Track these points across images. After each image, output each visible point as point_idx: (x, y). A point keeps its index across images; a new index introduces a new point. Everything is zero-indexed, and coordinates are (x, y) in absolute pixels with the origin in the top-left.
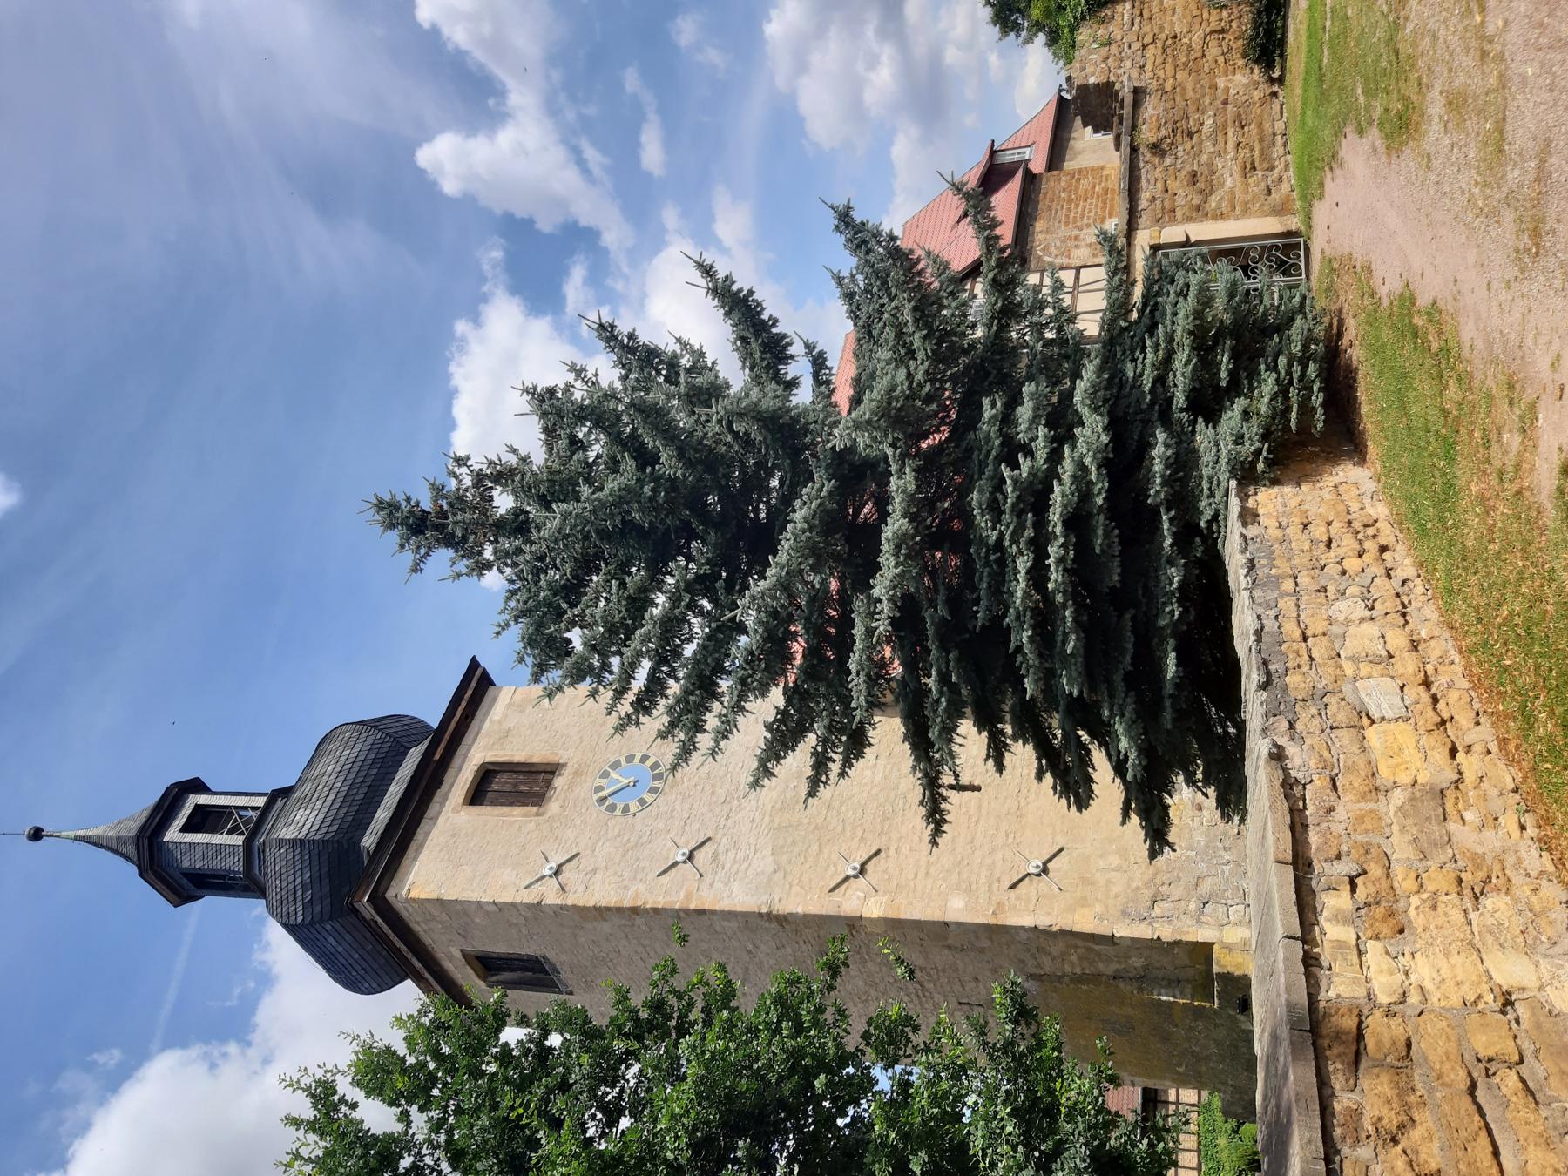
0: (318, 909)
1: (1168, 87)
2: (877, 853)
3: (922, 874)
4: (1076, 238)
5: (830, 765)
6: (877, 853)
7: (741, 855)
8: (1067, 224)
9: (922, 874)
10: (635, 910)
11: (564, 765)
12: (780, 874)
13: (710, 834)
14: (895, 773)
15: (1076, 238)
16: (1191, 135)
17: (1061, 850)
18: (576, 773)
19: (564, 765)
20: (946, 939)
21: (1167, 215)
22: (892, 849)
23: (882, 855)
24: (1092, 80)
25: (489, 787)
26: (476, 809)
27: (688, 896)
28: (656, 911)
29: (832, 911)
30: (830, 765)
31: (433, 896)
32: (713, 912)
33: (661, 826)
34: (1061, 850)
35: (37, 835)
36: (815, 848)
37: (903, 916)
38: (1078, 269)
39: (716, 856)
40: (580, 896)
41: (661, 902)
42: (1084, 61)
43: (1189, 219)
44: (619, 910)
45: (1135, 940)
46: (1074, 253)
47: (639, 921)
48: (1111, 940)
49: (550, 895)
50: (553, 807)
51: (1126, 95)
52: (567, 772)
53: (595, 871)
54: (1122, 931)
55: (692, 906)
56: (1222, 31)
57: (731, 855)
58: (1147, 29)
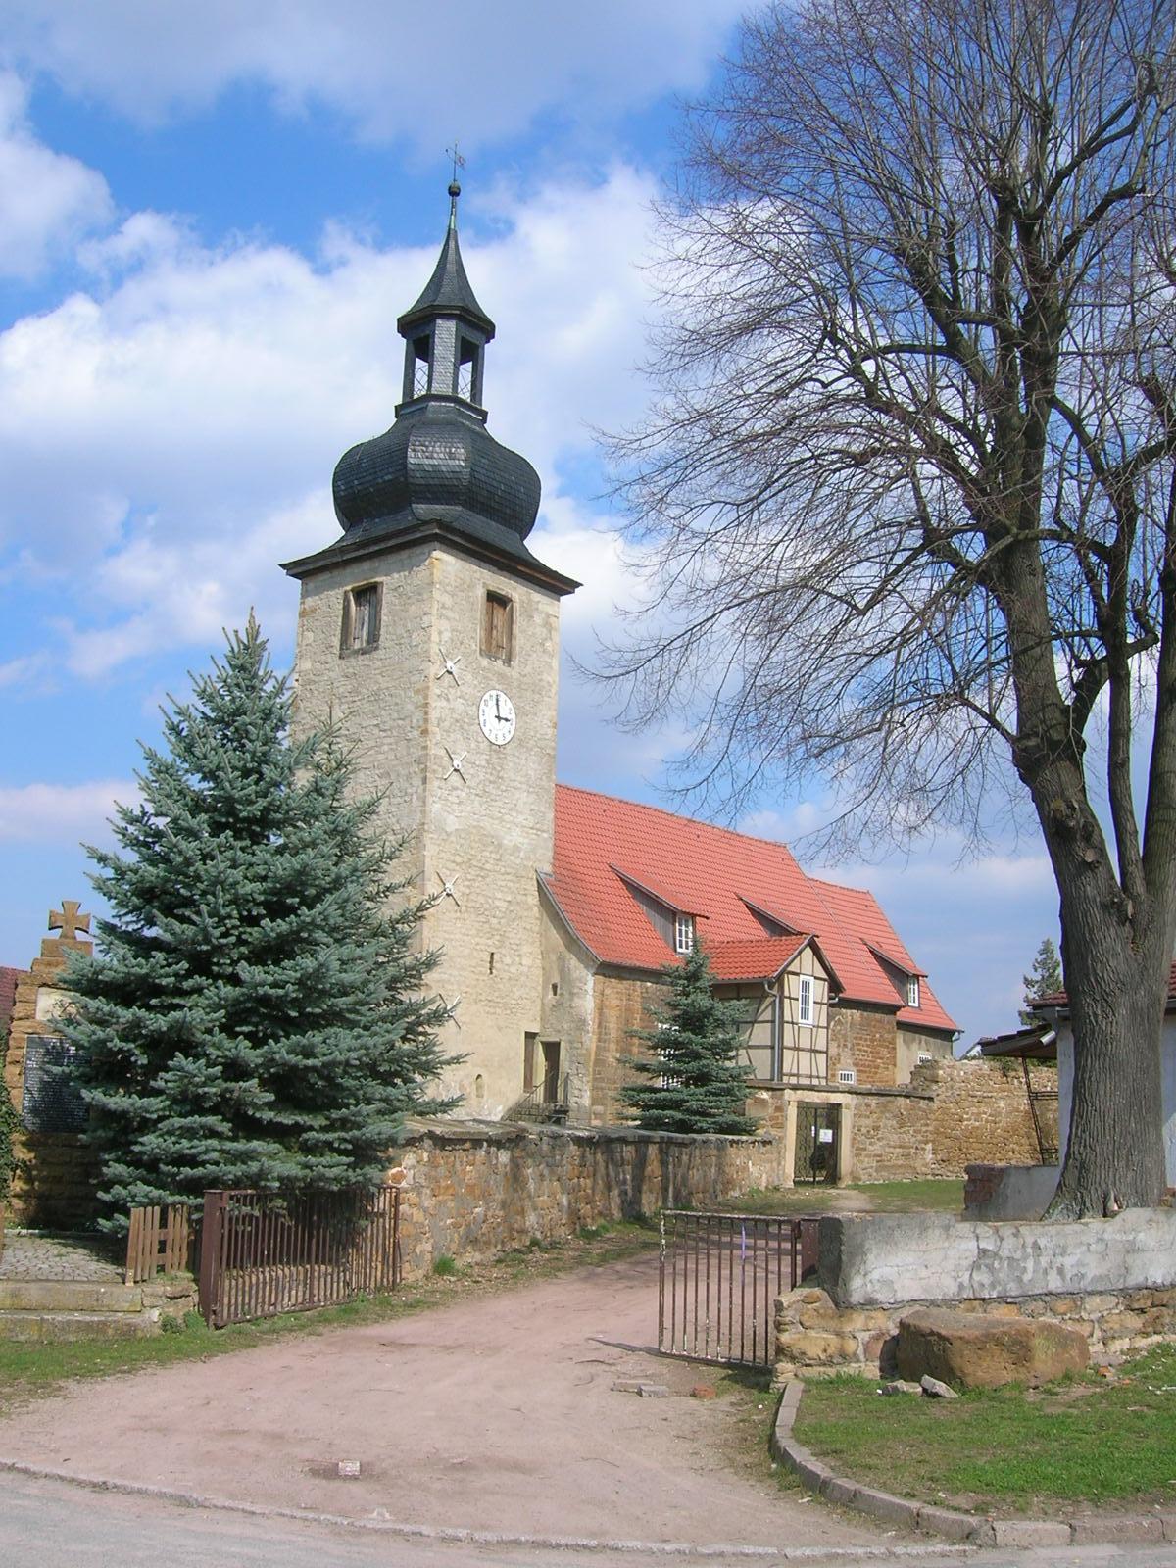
11: (509, 666)
23: (456, 908)
33: (473, 745)
50: (485, 662)
53: (448, 700)
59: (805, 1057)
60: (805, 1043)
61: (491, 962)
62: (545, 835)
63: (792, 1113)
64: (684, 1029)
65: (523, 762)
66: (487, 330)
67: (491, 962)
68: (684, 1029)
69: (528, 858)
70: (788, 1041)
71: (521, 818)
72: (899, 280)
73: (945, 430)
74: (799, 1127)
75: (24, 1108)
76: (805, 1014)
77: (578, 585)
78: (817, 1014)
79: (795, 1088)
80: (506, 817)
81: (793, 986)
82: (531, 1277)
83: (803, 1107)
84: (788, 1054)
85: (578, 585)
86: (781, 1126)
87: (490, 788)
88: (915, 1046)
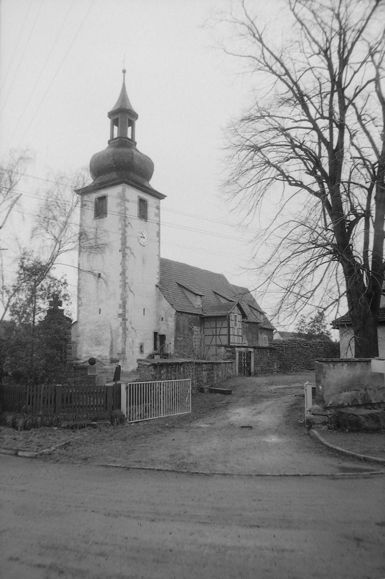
25: (142, 203)
59: (236, 338)
60: (236, 334)
63: (237, 354)
64: (322, 365)
66: (135, 116)
68: (322, 365)
70: (231, 333)
72: (84, 184)
73: (369, 72)
74: (239, 359)
75: (187, 435)
76: (236, 325)
77: (166, 196)
78: (239, 325)
79: (238, 347)
81: (232, 317)
82: (18, 281)
83: (240, 354)
84: (231, 337)
85: (166, 196)
86: (235, 359)
88: (263, 334)
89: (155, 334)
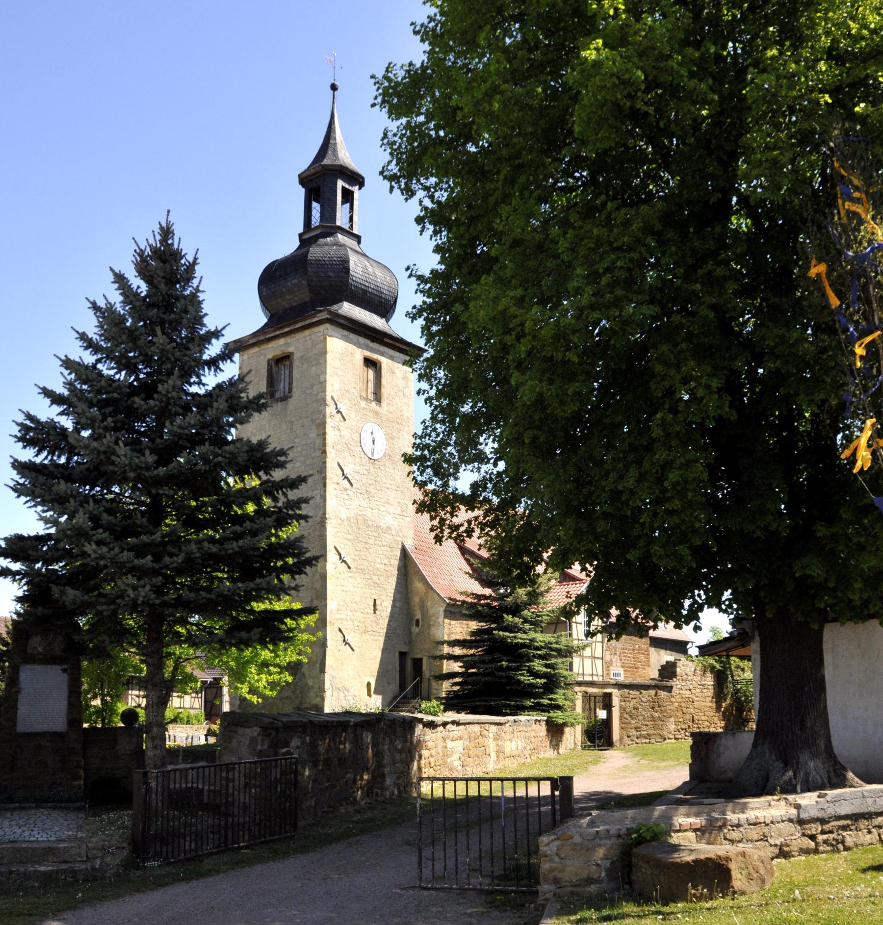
0: (315, 279)
1: (672, 699)
2: (349, 568)
3: (343, 588)
4: (615, 654)
5: (68, 371)
6: (349, 568)
7: (346, 501)
8: (622, 649)
9: (343, 588)
10: (324, 452)
11: (380, 406)
12: (340, 522)
13: (354, 485)
14: (380, 573)
15: (615, 654)
16: (653, 708)
17: (353, 650)
18: (376, 413)
19: (380, 406)
20: (317, 599)
21: (624, 699)
22: (350, 574)
24: (678, 669)
26: (362, 362)
27: (331, 478)
28: (325, 462)
29: (328, 549)
30: (68, 371)
31: (328, 349)
32: (325, 491)
34: (353, 650)
35: (334, 88)
36: (350, 537)
37: (328, 581)
38: (602, 659)
39: (346, 490)
40: (330, 423)
41: (328, 465)
42: (687, 665)
43: (621, 707)
44: (325, 445)
45: (324, 681)
46: (608, 653)
47: (318, 453)
48: (323, 671)
49: (330, 410)
51: (671, 683)
52: (378, 408)
53: (339, 430)
54: (327, 677)
55: (327, 481)
56: (693, 721)
57: (346, 497)
58: (698, 690)
61: (375, 605)
62: (408, 519)
65: (392, 471)
67: (375, 605)
69: (398, 535)
71: (391, 509)
80: (382, 509)
87: (370, 489)
89: (403, 655)
